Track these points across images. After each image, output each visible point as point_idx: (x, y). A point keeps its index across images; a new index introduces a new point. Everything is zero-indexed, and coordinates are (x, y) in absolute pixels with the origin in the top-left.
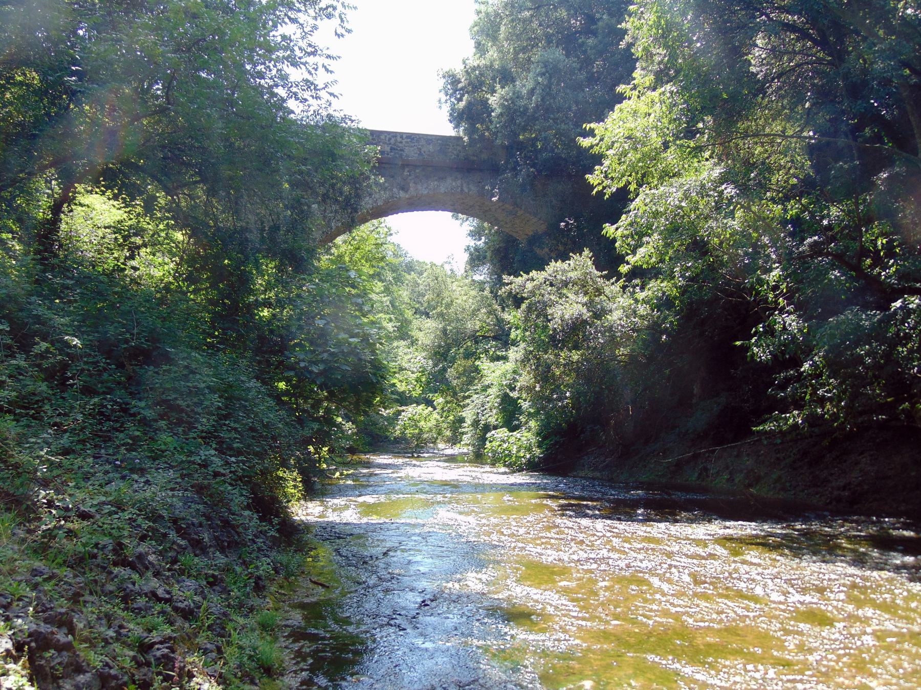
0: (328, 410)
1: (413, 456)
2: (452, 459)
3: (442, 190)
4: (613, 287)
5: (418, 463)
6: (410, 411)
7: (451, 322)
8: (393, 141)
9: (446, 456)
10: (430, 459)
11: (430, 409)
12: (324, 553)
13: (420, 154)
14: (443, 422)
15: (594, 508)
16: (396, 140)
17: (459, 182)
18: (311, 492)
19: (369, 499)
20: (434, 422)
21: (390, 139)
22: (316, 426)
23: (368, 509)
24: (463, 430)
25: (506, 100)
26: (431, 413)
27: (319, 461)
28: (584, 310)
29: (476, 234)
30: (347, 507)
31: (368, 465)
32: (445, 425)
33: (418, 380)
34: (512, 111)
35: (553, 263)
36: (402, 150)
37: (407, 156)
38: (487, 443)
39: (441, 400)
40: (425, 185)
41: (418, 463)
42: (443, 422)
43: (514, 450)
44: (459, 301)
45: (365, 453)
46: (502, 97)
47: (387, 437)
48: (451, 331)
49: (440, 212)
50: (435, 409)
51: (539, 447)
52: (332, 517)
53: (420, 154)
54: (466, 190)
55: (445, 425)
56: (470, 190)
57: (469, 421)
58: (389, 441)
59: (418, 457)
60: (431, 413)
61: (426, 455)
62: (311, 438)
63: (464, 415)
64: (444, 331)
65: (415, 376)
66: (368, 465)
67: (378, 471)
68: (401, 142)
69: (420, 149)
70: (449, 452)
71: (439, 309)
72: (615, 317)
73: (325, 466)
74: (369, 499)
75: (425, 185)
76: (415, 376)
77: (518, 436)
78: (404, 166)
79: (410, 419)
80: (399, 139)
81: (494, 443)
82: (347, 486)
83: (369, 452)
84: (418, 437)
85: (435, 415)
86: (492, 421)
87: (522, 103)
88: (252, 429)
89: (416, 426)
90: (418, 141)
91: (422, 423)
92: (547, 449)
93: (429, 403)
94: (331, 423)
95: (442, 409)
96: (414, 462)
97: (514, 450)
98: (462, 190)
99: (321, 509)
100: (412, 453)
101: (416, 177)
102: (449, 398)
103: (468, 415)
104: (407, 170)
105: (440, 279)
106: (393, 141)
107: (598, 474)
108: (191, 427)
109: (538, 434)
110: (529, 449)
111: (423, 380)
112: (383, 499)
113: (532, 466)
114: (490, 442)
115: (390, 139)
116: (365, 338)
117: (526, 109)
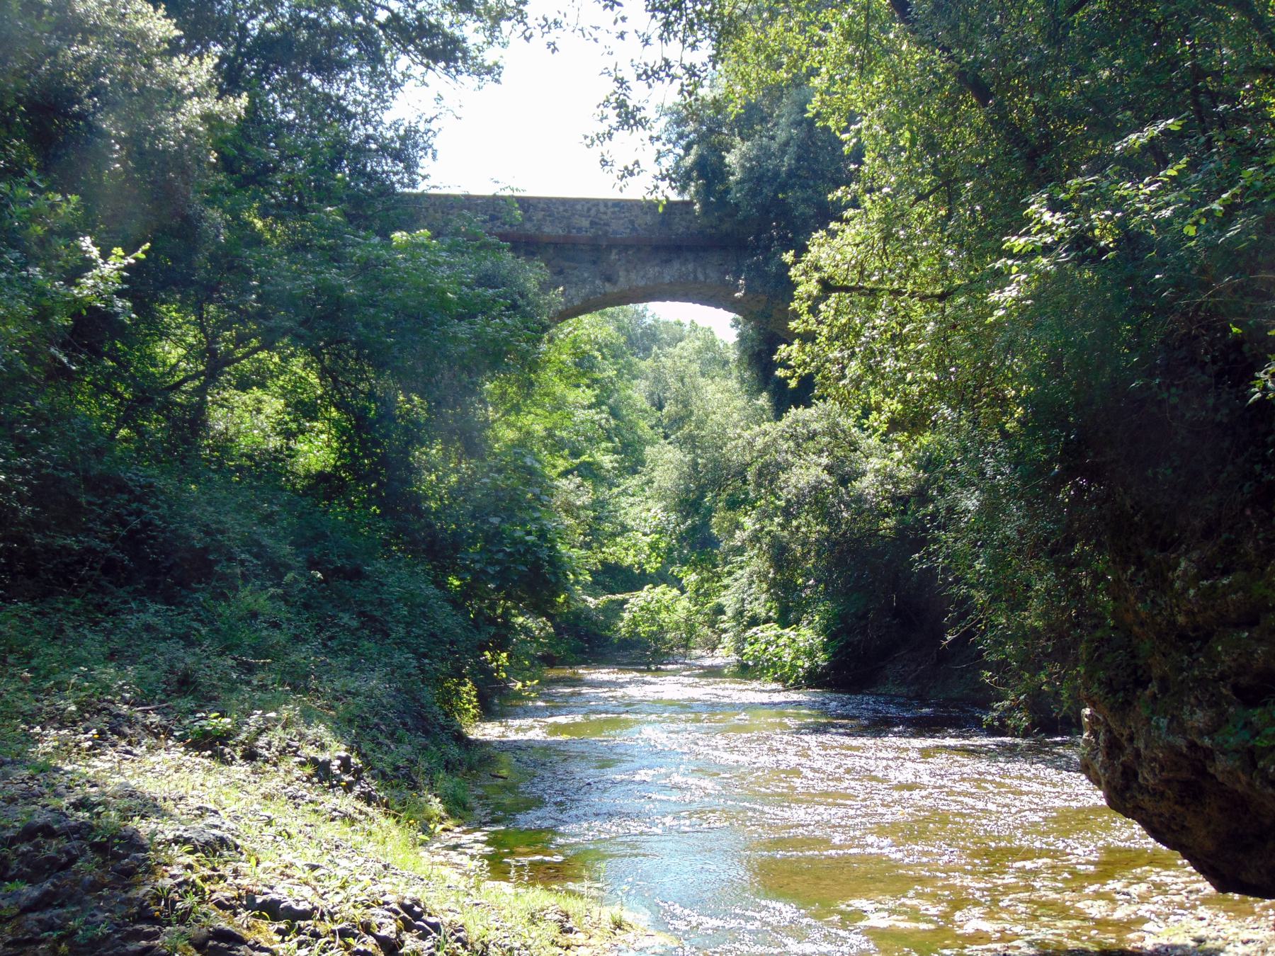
0: (506, 611)
1: (649, 670)
2: (713, 672)
3: (667, 279)
4: (870, 441)
5: (653, 680)
6: (638, 599)
7: (704, 449)
8: (593, 212)
9: (702, 667)
10: (674, 673)
11: (675, 592)
12: (506, 758)
13: (634, 229)
14: (698, 612)
15: (841, 726)
16: (598, 211)
17: (690, 267)
18: (488, 712)
19: (562, 720)
20: (684, 614)
21: (589, 210)
22: (493, 630)
23: (557, 729)
24: (722, 626)
25: (750, 160)
26: (675, 600)
27: (497, 671)
28: (825, 476)
29: (736, 323)
30: (532, 727)
31: (576, 682)
32: (701, 618)
33: (653, 547)
34: (757, 176)
35: (793, 410)
36: (607, 224)
37: (615, 232)
38: (747, 645)
39: (693, 577)
40: (642, 273)
41: (653, 680)
42: (698, 612)
43: (787, 656)
44: (717, 417)
45: (571, 665)
46: (743, 156)
47: (607, 639)
48: (705, 466)
49: (668, 303)
50: (683, 591)
51: (825, 650)
52: (512, 736)
53: (634, 229)
54: (701, 277)
55: (701, 618)
56: (706, 276)
57: (730, 612)
58: (612, 644)
59: (658, 670)
60: (675, 600)
61: (670, 667)
62: (487, 643)
63: (722, 600)
64: (695, 465)
65: (648, 539)
66: (576, 682)
67: (585, 690)
68: (605, 213)
69: (632, 222)
70: (708, 662)
71: (686, 430)
72: (866, 484)
73: (504, 675)
74: (562, 720)
75: (642, 273)
76: (648, 539)
77: (792, 634)
78: (610, 247)
79: (642, 609)
80: (602, 209)
81: (756, 646)
82: (537, 708)
83: (579, 664)
84: (658, 636)
85: (684, 602)
86: (762, 612)
87: (770, 164)
88: (433, 635)
89: (653, 619)
90: (629, 210)
91: (663, 615)
92: (834, 655)
93: (676, 582)
94: (508, 626)
95: (697, 591)
96: (648, 678)
97: (787, 656)
98: (696, 278)
99: (502, 729)
100: (648, 664)
101: (628, 262)
102: (705, 574)
103: (729, 600)
104: (614, 252)
105: (687, 380)
106: (593, 212)
107: (904, 690)
108: (388, 636)
109: (824, 630)
110: (811, 654)
111: (662, 545)
112: (579, 718)
113: (813, 679)
114: (751, 644)
115: (589, 210)
116: (542, 535)
117: (777, 174)
